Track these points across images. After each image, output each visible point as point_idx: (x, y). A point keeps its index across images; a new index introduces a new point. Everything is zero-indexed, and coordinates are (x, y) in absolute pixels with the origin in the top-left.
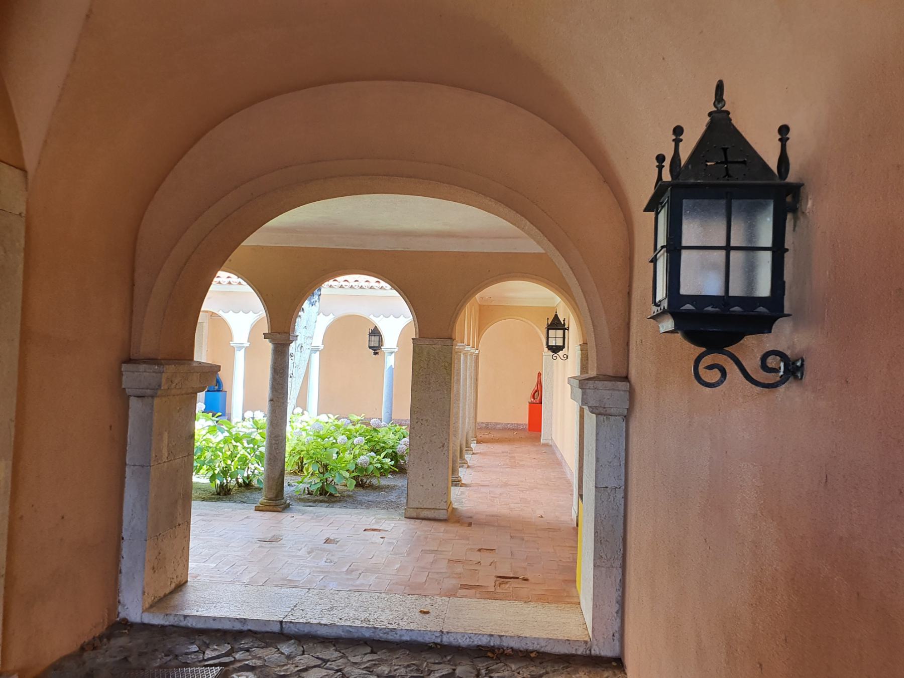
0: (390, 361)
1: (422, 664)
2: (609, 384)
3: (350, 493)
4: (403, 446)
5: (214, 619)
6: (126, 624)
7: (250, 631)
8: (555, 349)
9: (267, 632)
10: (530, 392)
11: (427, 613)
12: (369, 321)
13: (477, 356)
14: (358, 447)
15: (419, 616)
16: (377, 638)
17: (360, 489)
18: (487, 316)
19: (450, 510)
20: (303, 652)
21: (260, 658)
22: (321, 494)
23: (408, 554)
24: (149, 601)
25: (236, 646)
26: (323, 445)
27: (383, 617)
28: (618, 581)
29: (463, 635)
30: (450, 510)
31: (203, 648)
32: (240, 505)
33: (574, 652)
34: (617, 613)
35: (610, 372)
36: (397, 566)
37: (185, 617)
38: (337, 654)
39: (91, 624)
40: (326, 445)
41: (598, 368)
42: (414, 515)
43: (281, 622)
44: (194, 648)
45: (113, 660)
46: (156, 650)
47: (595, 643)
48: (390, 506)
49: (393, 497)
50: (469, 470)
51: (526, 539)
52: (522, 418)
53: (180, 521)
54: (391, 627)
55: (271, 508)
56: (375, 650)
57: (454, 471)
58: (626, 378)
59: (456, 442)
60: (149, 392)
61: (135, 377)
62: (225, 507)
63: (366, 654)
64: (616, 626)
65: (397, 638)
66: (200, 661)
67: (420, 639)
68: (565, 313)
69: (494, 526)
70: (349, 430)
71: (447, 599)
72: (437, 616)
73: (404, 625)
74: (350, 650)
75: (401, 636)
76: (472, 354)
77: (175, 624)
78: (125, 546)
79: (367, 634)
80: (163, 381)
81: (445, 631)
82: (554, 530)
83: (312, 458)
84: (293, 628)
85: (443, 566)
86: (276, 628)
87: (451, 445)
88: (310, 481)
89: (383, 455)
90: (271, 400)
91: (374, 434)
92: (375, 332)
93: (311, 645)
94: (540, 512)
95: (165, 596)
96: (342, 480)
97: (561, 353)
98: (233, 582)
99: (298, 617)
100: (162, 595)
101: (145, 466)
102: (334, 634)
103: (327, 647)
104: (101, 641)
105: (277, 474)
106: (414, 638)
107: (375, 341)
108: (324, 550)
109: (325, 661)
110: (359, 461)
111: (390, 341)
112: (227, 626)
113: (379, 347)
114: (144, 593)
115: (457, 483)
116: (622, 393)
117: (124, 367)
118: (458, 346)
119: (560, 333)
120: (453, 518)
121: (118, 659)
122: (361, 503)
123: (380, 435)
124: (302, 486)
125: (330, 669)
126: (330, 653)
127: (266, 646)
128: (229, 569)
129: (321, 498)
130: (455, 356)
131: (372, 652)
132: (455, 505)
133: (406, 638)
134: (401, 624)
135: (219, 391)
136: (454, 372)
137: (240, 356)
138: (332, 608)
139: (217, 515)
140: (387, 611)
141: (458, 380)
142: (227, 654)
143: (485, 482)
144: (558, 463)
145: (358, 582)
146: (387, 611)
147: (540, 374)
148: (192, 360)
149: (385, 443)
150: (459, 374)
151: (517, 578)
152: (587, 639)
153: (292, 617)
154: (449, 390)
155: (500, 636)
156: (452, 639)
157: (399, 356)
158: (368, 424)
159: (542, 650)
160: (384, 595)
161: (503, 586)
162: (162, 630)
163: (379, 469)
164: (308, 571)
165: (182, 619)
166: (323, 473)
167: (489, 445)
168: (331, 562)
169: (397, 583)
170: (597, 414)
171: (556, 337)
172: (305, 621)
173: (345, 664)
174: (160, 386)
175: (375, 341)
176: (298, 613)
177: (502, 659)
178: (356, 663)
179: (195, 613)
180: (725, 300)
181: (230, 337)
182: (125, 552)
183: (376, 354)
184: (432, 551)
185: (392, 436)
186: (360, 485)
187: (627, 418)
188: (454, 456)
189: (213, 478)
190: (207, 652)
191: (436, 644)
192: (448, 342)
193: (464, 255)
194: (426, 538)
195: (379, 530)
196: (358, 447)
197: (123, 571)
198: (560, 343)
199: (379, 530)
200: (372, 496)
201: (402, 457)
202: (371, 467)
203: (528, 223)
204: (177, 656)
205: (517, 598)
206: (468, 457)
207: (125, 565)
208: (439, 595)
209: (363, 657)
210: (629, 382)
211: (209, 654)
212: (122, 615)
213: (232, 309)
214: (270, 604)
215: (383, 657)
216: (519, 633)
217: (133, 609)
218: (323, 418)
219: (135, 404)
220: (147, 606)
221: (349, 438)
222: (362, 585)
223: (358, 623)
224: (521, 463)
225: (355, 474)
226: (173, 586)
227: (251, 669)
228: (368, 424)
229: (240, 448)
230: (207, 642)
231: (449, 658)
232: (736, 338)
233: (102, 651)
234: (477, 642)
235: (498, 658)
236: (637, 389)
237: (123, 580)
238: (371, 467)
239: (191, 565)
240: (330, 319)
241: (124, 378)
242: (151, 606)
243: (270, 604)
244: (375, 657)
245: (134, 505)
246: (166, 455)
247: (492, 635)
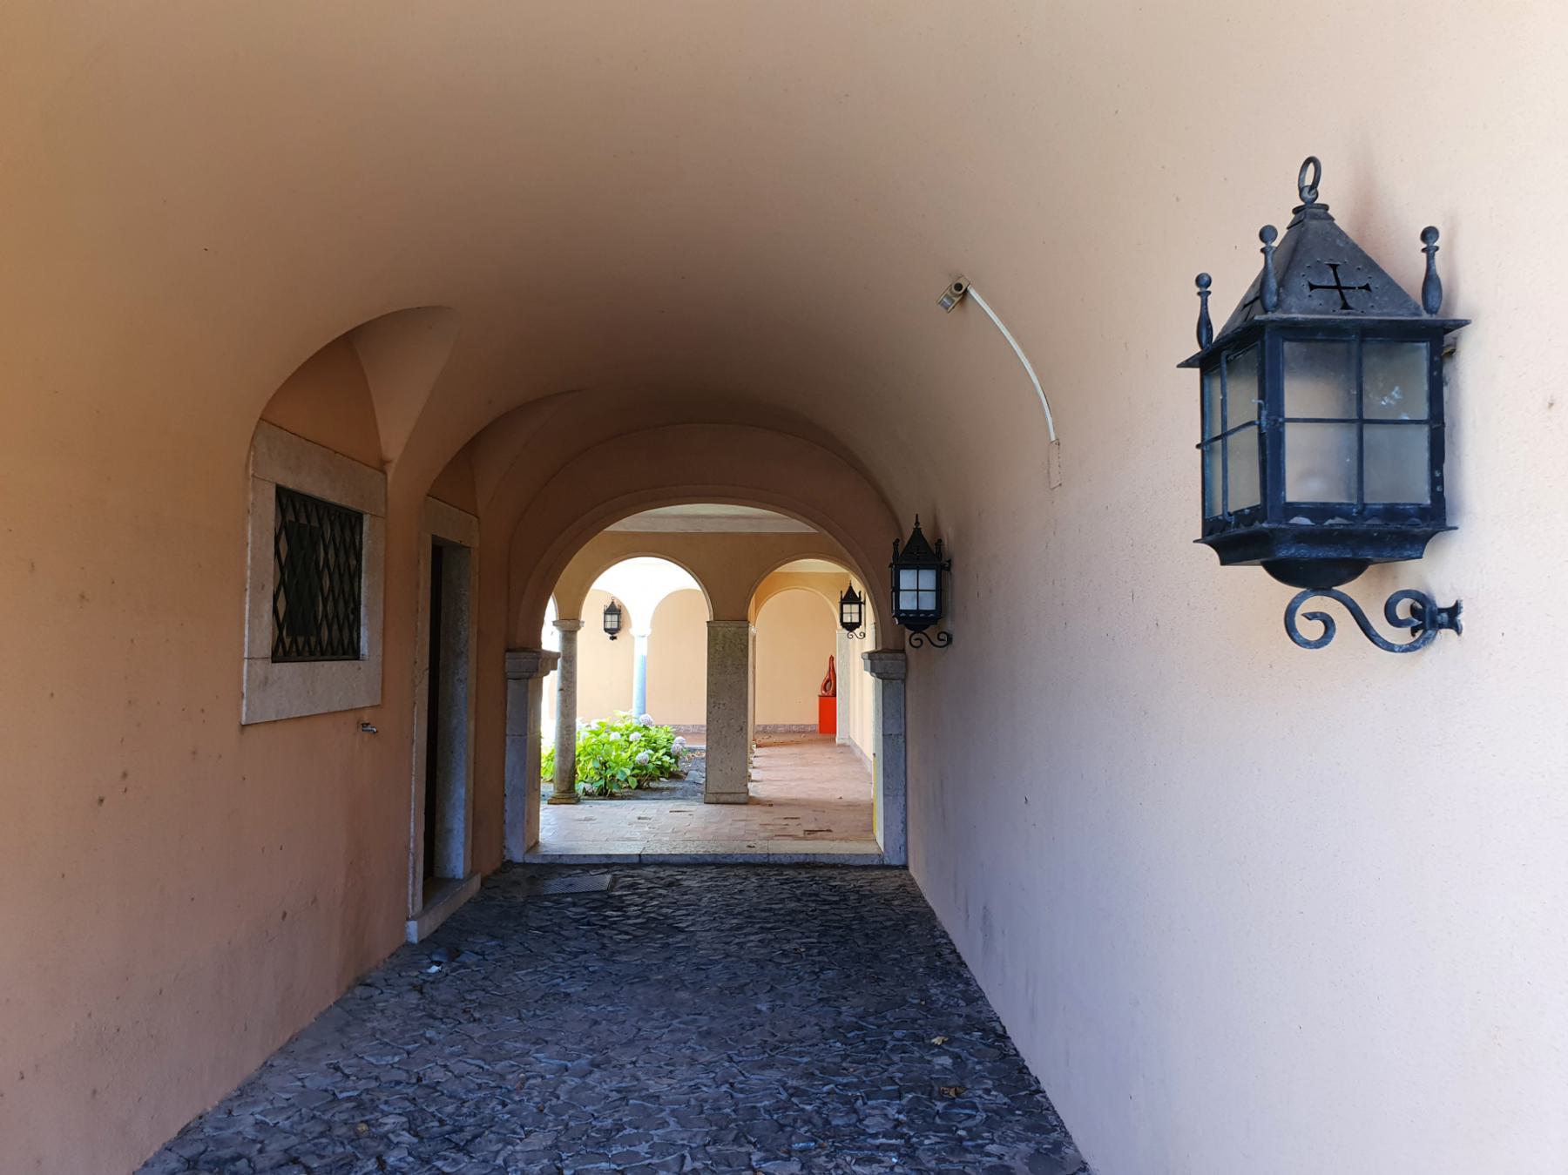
8: (851, 627)
42: (713, 799)
52: (812, 718)
64: (902, 841)
68: (858, 587)
78: (507, 800)
86: (636, 860)
97: (857, 631)
105: (569, 765)
107: (612, 621)
119: (855, 608)
120: (750, 801)
144: (859, 761)
147: (832, 659)
175: (612, 625)
180: (918, 611)
183: (613, 638)
187: (904, 681)
192: (743, 624)
198: (856, 620)
217: (518, 855)
232: (1355, 568)
237: (507, 830)
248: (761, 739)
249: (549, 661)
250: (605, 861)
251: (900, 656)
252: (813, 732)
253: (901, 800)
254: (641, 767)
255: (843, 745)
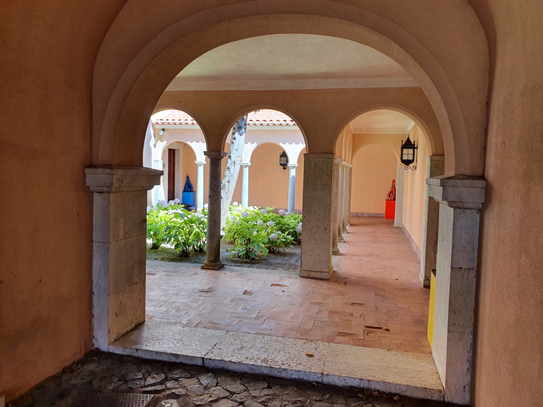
0: (293, 173)
1: (306, 401)
2: (467, 182)
3: (265, 258)
4: (299, 228)
5: (157, 353)
6: (98, 353)
7: (181, 363)
8: (407, 162)
9: (193, 365)
10: (387, 192)
11: (311, 356)
12: (281, 148)
13: (351, 169)
14: (270, 228)
15: (305, 358)
16: (273, 374)
17: (272, 255)
18: (358, 141)
19: (331, 273)
20: (217, 383)
21: (184, 387)
22: (246, 258)
23: (300, 305)
24: (114, 337)
25: (170, 376)
26: (247, 226)
27: (278, 358)
28: (469, 344)
29: (339, 377)
30: (331, 273)
31: (146, 375)
32: (192, 265)
33: (430, 398)
34: (468, 370)
35: (468, 172)
36: (292, 315)
37: (137, 350)
38: (242, 388)
39: (70, 352)
40: (249, 226)
41: (456, 169)
42: (306, 275)
43: (203, 358)
44: (140, 376)
45: (82, 381)
46: (114, 375)
47: (448, 392)
48: (291, 267)
49: (293, 261)
50: (345, 244)
51: (386, 296)
52: (382, 210)
53: (136, 279)
54: (283, 367)
55: (211, 267)
56: (271, 385)
57: (334, 245)
58: (482, 177)
59: (334, 227)
60: (105, 189)
61: (95, 178)
62: (184, 266)
63: (264, 389)
64: (467, 380)
65: (288, 376)
66: (142, 387)
67: (305, 378)
69: (362, 285)
70: (265, 217)
71: (327, 344)
72: (319, 359)
73: (294, 366)
74: (252, 384)
75: (291, 375)
76: (347, 167)
77: (131, 354)
78: (95, 297)
79: (266, 372)
80: (115, 181)
81: (325, 373)
82: (407, 290)
83: (239, 234)
84: (211, 364)
85: (325, 316)
86: (200, 363)
87: (332, 229)
88: (240, 249)
89: (286, 233)
90: (210, 197)
91: (281, 219)
92: (284, 155)
93: (223, 378)
94: (395, 276)
95: (127, 332)
96: (260, 250)
97: (411, 165)
98: (176, 323)
99: (215, 355)
100: (124, 332)
101: (106, 242)
102: (241, 370)
103: (234, 381)
104: (77, 366)
105: (215, 244)
106: (301, 377)
108: (242, 300)
109: (232, 393)
110: (271, 237)
111: (294, 159)
112: (166, 358)
113: (286, 165)
114: (109, 331)
115: (336, 253)
116: (479, 190)
117: (87, 171)
118: (336, 161)
119: (411, 151)
120: (333, 278)
121: (85, 381)
122: (272, 264)
123: (285, 220)
124: (233, 252)
125: (235, 401)
126: (236, 386)
127: (191, 377)
128: (176, 313)
129: (246, 260)
130: (335, 168)
131: (269, 387)
132: (335, 269)
133: (295, 376)
134: (291, 364)
135: (190, 191)
136: (334, 179)
137: (201, 170)
138: (242, 348)
139: (176, 272)
140: (282, 353)
141: (337, 185)
142: (161, 383)
143: (354, 254)
145: (262, 327)
146: (282, 353)
147: (394, 181)
148: (142, 166)
149: (288, 225)
150: (337, 180)
151: (381, 328)
152: (441, 388)
153: (211, 355)
154: (330, 190)
155: (369, 381)
156: (330, 380)
157: (297, 169)
158: (277, 213)
159: (403, 394)
160: (280, 339)
161: (370, 334)
162: (121, 358)
163: (284, 242)
164: (229, 315)
165: (135, 351)
166: (247, 244)
167: (358, 227)
168: (246, 309)
169: (291, 329)
170: (455, 208)
171: (408, 154)
172: (220, 359)
173: (247, 397)
174: (112, 184)
176: (216, 351)
177: (371, 399)
178: (255, 397)
179: (144, 348)
181: (195, 159)
182: (95, 303)
183: (284, 168)
184: (318, 304)
185: (293, 221)
186: (272, 252)
187: (482, 211)
188: (334, 233)
189: (177, 246)
190: (148, 379)
191: (318, 383)
192: (330, 156)
193: (343, 91)
194: (314, 293)
195: (282, 286)
196: (270, 228)
197: (95, 315)
198: (411, 158)
199: (282, 286)
200: (279, 260)
201: (300, 234)
202: (279, 241)
203: (397, 47)
204: (126, 382)
205: (381, 346)
206: (344, 235)
207: (96, 311)
208: (322, 340)
209: (260, 391)
210: (485, 180)
211: (150, 381)
212: (95, 346)
213: (169, 129)
214: (198, 343)
215: (276, 392)
216: (384, 378)
217: (103, 342)
218: (251, 208)
219: (98, 199)
220: (113, 340)
221: (265, 222)
222: (265, 329)
223: (259, 363)
224: (381, 240)
225: (267, 245)
226: (133, 325)
227: (176, 396)
228: (277, 213)
229: (195, 227)
230: (150, 370)
231: (327, 396)
233: (76, 374)
234: (350, 383)
235: (367, 399)
236: (496, 186)
237: (95, 322)
238: (279, 241)
239: (147, 308)
240: (255, 145)
241: (87, 179)
242: (116, 340)
243: (198, 343)
244: (270, 392)
245: (100, 270)
246: (122, 234)
247: (362, 379)
248: (353, 221)
249: (154, 177)
250: (173, 359)
251: (480, 183)
252: (382, 217)
253: (469, 339)
254: (271, 242)
255: (398, 228)
